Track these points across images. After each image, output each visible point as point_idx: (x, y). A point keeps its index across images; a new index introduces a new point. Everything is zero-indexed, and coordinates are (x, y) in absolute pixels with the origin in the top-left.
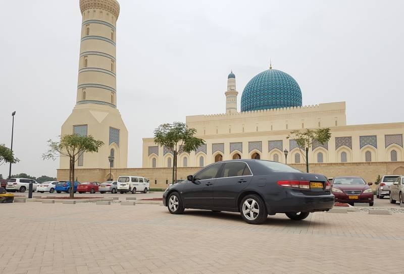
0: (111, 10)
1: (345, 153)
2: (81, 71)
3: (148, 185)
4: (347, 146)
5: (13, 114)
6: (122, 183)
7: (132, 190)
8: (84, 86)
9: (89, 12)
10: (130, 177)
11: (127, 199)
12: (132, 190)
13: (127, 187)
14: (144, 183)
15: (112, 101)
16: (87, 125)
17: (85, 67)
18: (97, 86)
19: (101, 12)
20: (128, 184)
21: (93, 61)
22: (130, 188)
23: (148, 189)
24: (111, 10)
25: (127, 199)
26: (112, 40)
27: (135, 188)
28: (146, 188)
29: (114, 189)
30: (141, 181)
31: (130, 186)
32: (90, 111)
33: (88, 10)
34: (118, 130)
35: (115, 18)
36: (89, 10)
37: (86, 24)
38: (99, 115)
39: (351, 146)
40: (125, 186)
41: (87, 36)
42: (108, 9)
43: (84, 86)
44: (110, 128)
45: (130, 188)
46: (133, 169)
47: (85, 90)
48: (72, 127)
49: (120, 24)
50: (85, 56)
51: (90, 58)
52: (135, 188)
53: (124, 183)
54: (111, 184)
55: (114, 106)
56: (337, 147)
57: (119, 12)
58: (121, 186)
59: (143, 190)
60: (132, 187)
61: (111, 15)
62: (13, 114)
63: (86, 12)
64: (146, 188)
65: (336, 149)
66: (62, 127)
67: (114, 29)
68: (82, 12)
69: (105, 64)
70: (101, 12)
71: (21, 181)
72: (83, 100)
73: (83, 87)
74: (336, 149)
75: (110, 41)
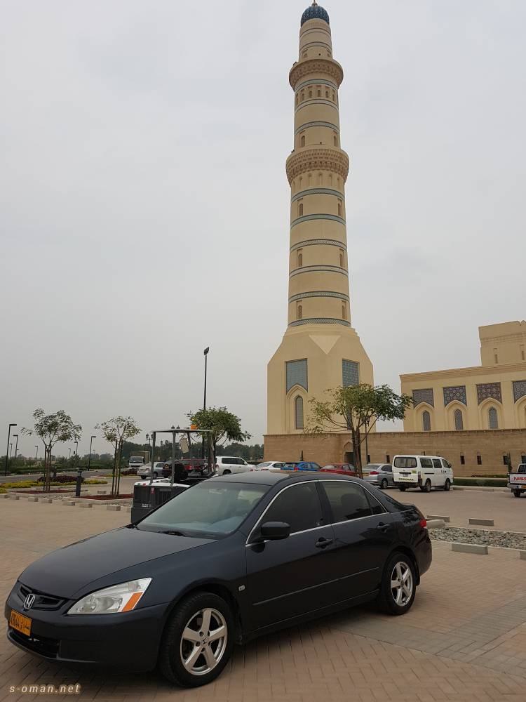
0: (335, 168)
1: (494, 409)
2: (294, 274)
3: (450, 474)
4: (493, 397)
5: (206, 352)
6: (402, 470)
7: (424, 484)
8: (299, 296)
9: (310, 176)
10: (418, 457)
11: (490, 523)
12: (424, 484)
13: (413, 478)
14: (444, 468)
15: (344, 316)
16: (306, 359)
17: (299, 266)
18: (311, 294)
19: (321, 174)
20: (414, 472)
21: (312, 256)
22: (420, 480)
23: (452, 481)
24: (335, 168)
25: (490, 523)
26: (339, 217)
27: (428, 480)
28: (448, 480)
29: (385, 479)
30: (438, 465)
31: (419, 476)
32: (310, 336)
33: (299, 176)
34: (357, 364)
35: (342, 179)
36: (302, 175)
37: (298, 200)
38: (324, 340)
39: (465, 397)
40: (409, 477)
41: (300, 215)
42: (331, 167)
43: (299, 296)
44: (343, 360)
45: (420, 480)
46: (391, 433)
47: (300, 304)
48: (284, 365)
49: (352, 188)
50: (297, 250)
51: (306, 251)
52: (428, 480)
53: (407, 470)
54: (379, 470)
55: (347, 323)
56: (480, 400)
57: (348, 169)
58: (402, 476)
59: (443, 484)
60: (424, 478)
61: (336, 176)
62: (206, 352)
63: (296, 180)
64: (448, 480)
65: (479, 403)
66: (268, 365)
67: (341, 198)
68: (290, 183)
69: (331, 258)
70: (321, 174)
71: (224, 461)
72: (298, 318)
73: (296, 300)
74: (479, 403)
75: (337, 219)
